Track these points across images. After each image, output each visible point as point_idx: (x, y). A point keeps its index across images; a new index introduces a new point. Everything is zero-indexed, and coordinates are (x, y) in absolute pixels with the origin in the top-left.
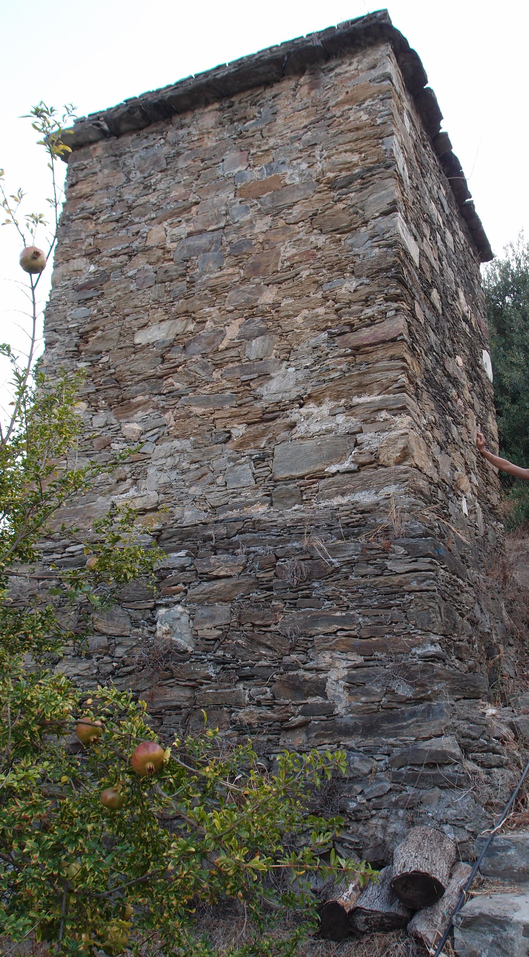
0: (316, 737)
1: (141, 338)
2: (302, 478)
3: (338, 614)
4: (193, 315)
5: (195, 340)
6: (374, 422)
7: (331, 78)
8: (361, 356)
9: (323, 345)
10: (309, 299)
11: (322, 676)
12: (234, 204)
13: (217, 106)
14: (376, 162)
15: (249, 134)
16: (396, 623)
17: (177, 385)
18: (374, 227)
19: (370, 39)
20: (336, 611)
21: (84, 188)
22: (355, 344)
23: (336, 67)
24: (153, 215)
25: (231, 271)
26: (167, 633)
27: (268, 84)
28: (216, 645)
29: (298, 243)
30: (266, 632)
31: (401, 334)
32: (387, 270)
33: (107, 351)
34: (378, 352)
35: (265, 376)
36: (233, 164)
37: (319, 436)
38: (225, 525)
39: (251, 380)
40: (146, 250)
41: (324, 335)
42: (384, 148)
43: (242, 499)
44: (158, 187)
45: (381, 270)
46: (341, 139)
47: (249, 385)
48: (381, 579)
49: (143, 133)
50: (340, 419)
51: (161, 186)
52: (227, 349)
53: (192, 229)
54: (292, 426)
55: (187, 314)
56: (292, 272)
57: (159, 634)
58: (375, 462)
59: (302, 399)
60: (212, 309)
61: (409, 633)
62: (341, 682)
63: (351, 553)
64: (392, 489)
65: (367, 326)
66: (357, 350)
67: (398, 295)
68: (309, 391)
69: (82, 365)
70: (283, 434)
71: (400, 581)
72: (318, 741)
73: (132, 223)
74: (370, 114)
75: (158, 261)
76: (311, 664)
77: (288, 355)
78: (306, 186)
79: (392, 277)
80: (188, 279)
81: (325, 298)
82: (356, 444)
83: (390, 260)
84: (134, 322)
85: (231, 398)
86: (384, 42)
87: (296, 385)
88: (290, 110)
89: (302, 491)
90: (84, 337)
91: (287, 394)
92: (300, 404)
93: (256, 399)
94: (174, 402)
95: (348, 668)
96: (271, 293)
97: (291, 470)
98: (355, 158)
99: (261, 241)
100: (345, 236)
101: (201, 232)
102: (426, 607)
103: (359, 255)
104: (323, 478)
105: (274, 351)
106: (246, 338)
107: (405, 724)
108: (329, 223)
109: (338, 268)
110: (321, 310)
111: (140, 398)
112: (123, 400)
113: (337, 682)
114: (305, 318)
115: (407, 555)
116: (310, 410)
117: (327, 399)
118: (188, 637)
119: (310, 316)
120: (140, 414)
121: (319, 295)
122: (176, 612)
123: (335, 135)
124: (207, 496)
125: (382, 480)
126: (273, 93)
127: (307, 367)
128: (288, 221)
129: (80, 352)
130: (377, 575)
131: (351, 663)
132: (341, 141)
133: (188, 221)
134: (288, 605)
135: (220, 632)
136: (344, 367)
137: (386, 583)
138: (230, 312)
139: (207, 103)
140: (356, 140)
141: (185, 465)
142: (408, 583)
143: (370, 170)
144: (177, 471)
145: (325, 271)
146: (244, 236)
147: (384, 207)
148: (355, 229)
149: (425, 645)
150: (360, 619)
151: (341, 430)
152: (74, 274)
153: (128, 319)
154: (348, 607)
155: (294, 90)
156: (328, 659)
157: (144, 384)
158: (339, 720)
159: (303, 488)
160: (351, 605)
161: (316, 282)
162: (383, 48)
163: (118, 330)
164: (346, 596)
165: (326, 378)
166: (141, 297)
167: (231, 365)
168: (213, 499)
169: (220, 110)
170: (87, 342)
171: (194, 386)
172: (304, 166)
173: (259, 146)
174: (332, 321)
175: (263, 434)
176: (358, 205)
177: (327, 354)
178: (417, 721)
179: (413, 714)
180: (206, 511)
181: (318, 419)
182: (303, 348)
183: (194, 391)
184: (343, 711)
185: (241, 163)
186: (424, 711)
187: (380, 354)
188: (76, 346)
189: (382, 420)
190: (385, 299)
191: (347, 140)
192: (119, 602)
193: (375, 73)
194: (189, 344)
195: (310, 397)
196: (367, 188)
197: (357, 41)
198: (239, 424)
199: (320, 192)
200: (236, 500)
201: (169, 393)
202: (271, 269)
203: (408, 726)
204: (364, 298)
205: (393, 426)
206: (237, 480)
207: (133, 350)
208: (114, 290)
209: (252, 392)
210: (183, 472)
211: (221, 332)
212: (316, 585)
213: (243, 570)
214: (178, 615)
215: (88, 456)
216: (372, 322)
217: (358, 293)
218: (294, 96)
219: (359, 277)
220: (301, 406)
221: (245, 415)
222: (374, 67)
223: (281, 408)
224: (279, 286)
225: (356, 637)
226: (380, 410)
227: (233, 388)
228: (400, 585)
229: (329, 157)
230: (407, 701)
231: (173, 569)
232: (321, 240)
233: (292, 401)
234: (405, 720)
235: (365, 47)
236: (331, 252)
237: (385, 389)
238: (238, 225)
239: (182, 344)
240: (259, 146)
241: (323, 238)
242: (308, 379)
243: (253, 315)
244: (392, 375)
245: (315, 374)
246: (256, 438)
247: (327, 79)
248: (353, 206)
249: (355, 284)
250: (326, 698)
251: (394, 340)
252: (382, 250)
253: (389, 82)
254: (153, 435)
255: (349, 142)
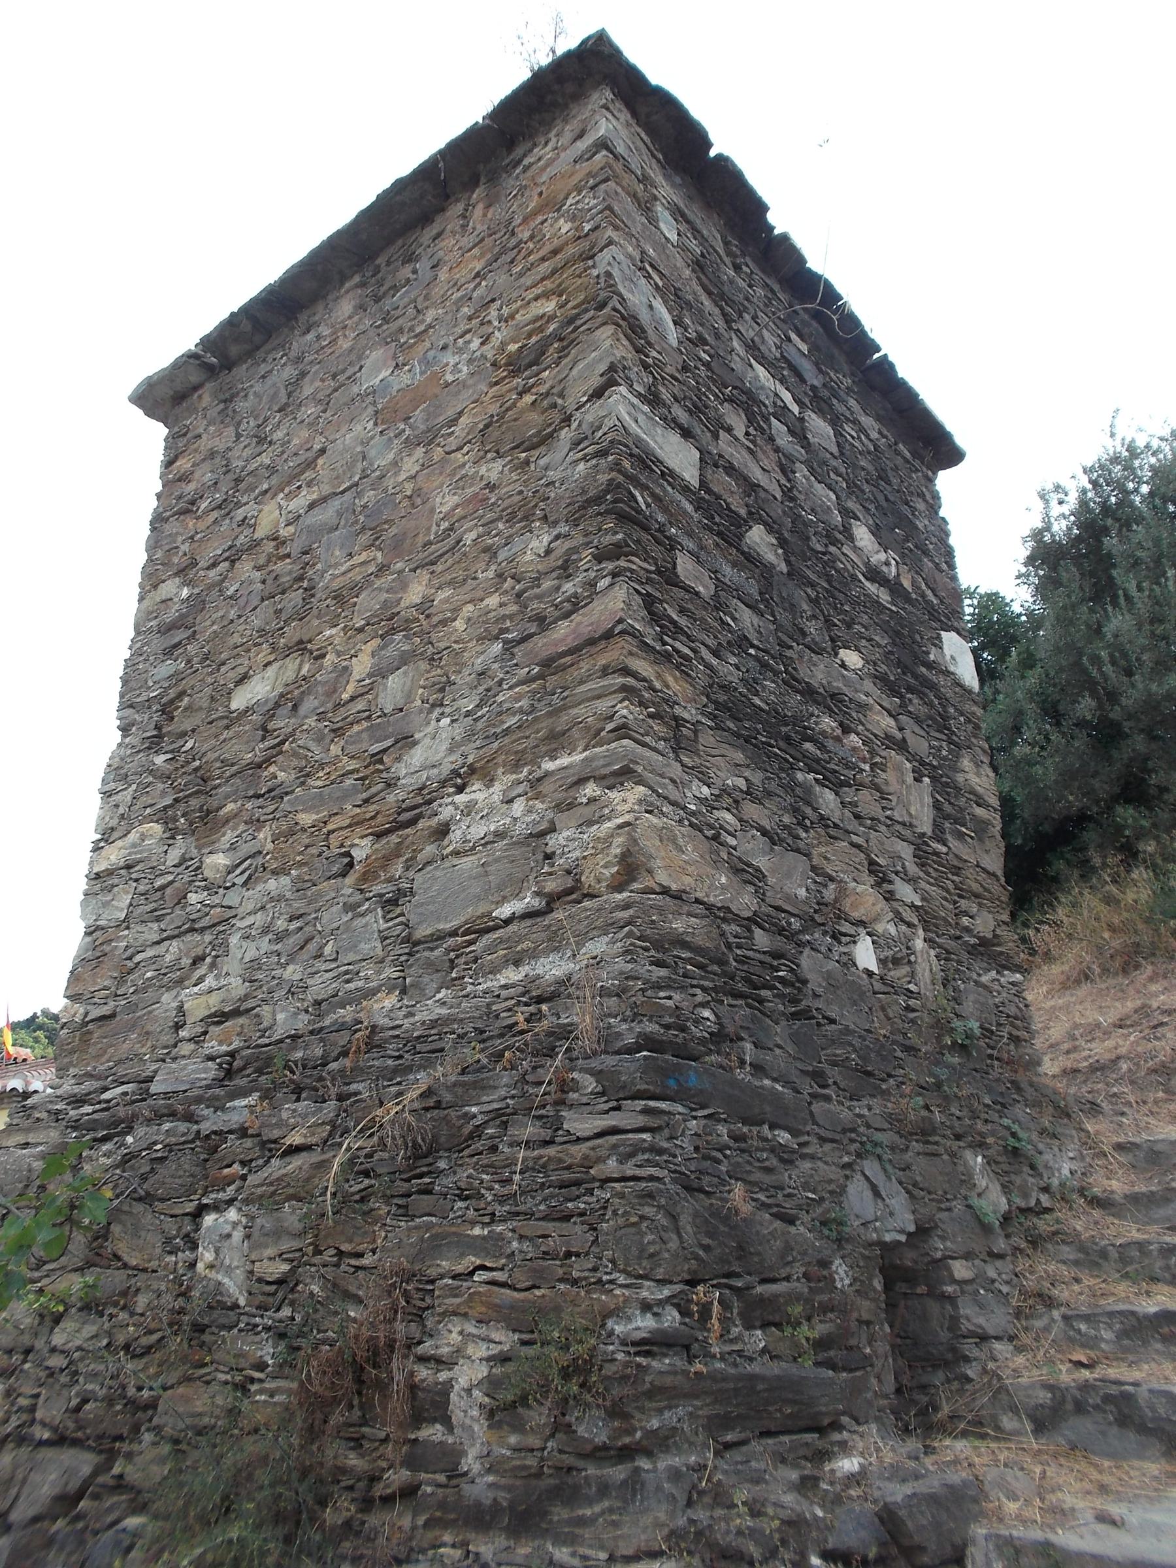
0: (426, 1525)
1: (238, 702)
2: (454, 933)
3: (477, 1231)
4: (309, 646)
5: (308, 692)
6: (571, 806)
7: (517, 177)
8: (554, 678)
9: (496, 666)
10: (475, 583)
11: (443, 1376)
12: (372, 438)
13: (357, 279)
14: (582, 303)
15: (399, 312)
16: (578, 1255)
17: (282, 775)
18: (580, 425)
19: (570, 88)
20: (473, 1223)
21: (183, 464)
22: (544, 654)
23: (525, 155)
24: (265, 486)
25: (363, 557)
26: (211, 1267)
27: (426, 219)
28: (280, 1295)
29: (461, 483)
30: (358, 1268)
31: (621, 621)
32: (598, 499)
33: (193, 731)
34: (582, 664)
35: (406, 741)
36: (377, 371)
37: (484, 845)
38: (322, 1040)
39: (385, 751)
40: (256, 544)
41: (497, 647)
42: (595, 272)
43: (360, 984)
44: (275, 437)
45: (589, 502)
46: (528, 281)
47: (381, 762)
48: (552, 1151)
49: (260, 354)
50: (518, 807)
51: (279, 434)
52: (353, 699)
53: (315, 496)
54: (443, 831)
55: (301, 647)
56: (451, 541)
57: (200, 1266)
58: (574, 891)
59: (459, 776)
60: (334, 631)
61: (600, 1281)
62: (476, 1393)
63: (503, 1092)
64: (598, 946)
65: (567, 615)
66: (549, 665)
67: (617, 545)
68: (470, 759)
69: (160, 760)
70: (428, 848)
71: (586, 1157)
72: (430, 1535)
73: (239, 505)
74: (573, 218)
75: (269, 561)
76: (426, 1348)
77: (439, 696)
78: (476, 378)
79: (607, 512)
80: (305, 584)
81: (500, 576)
82: (549, 856)
83: (603, 478)
84: (231, 674)
85: (355, 790)
86: (596, 86)
87: (451, 750)
88: (457, 254)
89: (452, 961)
90: (167, 711)
91: (436, 771)
92: (455, 786)
93: (389, 785)
94: (273, 807)
95: (489, 1359)
96: (420, 583)
97: (439, 920)
98: (550, 306)
99: (408, 493)
100: (536, 453)
101: (324, 499)
102: (634, 1219)
103: (553, 483)
104: (488, 930)
105: (421, 691)
106: (380, 673)
107: (588, 1512)
108: (509, 436)
109: (522, 515)
110: (493, 601)
111: (230, 807)
112: (209, 812)
113: (469, 1391)
114: (469, 619)
115: (603, 1094)
116: (473, 796)
117: (500, 770)
118: (239, 1274)
119: (476, 614)
120: (229, 836)
121: (490, 574)
122: (226, 1222)
123: (521, 275)
124: (310, 982)
125: (582, 927)
126: (435, 232)
127: (468, 714)
128: (447, 449)
129: (160, 736)
130: (547, 1143)
131: (495, 1350)
132: (529, 283)
133: (309, 485)
134: (394, 1208)
135: (285, 1267)
136: (524, 703)
137: (560, 1161)
138: (361, 630)
139: (343, 279)
140: (553, 273)
141: (281, 924)
142: (601, 1160)
143: (571, 321)
144: (270, 936)
145: (501, 526)
146: (385, 490)
147: (596, 381)
148: (551, 435)
149: (629, 1311)
150: (515, 1244)
151: (520, 829)
152: (163, 606)
153: (223, 669)
154: (493, 1214)
155: (465, 217)
156: (455, 1338)
157: (237, 781)
158: (467, 1489)
159: (452, 955)
160: (500, 1210)
161: (486, 550)
162: (595, 96)
163: (208, 690)
164: (491, 1189)
165: (498, 730)
166: (241, 628)
167: (356, 728)
168: (319, 986)
169: (363, 285)
170: (172, 718)
171: (304, 776)
172: (476, 343)
173: (411, 329)
174: (511, 617)
175: (396, 853)
176: (555, 391)
177: (500, 683)
178: (611, 1510)
179: (604, 1489)
180: (307, 1011)
181: (489, 810)
182: (463, 678)
183: (303, 783)
184: (476, 1467)
185: (385, 364)
186: (624, 1483)
187: (585, 666)
188: (156, 727)
189: (585, 800)
190: (595, 557)
191: (539, 277)
192: (147, 1199)
193: (582, 145)
194: (302, 700)
195: (472, 770)
196: (566, 356)
197: (549, 98)
198: (362, 837)
199: (496, 383)
200: (352, 986)
201: (269, 791)
202: (421, 540)
203: (592, 1520)
204: (560, 562)
205: (606, 811)
206: (353, 947)
207: (226, 722)
208: (208, 623)
209: (384, 775)
210: (280, 937)
211: (346, 668)
212: (442, 1164)
213: (331, 1134)
214: (228, 1229)
215: (158, 919)
216: (575, 605)
217: (553, 556)
218: (464, 227)
219: (555, 523)
220: (460, 789)
221: (372, 818)
222: (580, 136)
223: (426, 798)
224: (434, 568)
225: (503, 1285)
226: (581, 781)
227: (357, 771)
228: (587, 1164)
229: (512, 316)
230: (599, 1454)
231: (230, 1132)
232: (493, 470)
233: (443, 783)
234: (590, 1502)
235: (566, 106)
236: (511, 488)
237: (595, 737)
238: (377, 473)
239: (291, 700)
240: (411, 329)
241: (498, 465)
242: (470, 735)
243: (393, 631)
244: (602, 706)
245: (480, 725)
246: (387, 859)
247: (510, 183)
248: (548, 394)
249: (546, 539)
250: (450, 1428)
251: (608, 635)
252: (589, 464)
253: (604, 152)
254: (242, 873)
255: (543, 279)
